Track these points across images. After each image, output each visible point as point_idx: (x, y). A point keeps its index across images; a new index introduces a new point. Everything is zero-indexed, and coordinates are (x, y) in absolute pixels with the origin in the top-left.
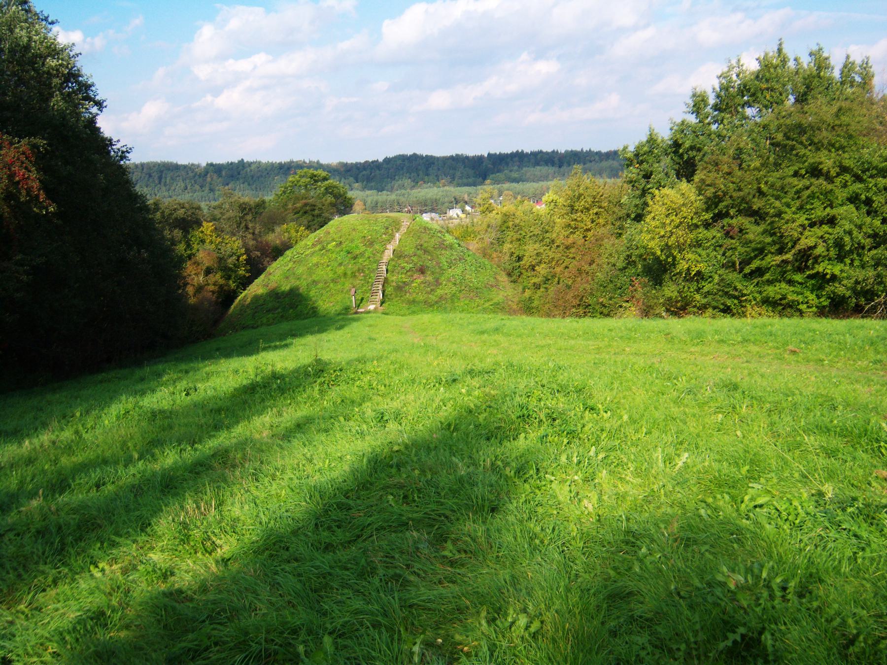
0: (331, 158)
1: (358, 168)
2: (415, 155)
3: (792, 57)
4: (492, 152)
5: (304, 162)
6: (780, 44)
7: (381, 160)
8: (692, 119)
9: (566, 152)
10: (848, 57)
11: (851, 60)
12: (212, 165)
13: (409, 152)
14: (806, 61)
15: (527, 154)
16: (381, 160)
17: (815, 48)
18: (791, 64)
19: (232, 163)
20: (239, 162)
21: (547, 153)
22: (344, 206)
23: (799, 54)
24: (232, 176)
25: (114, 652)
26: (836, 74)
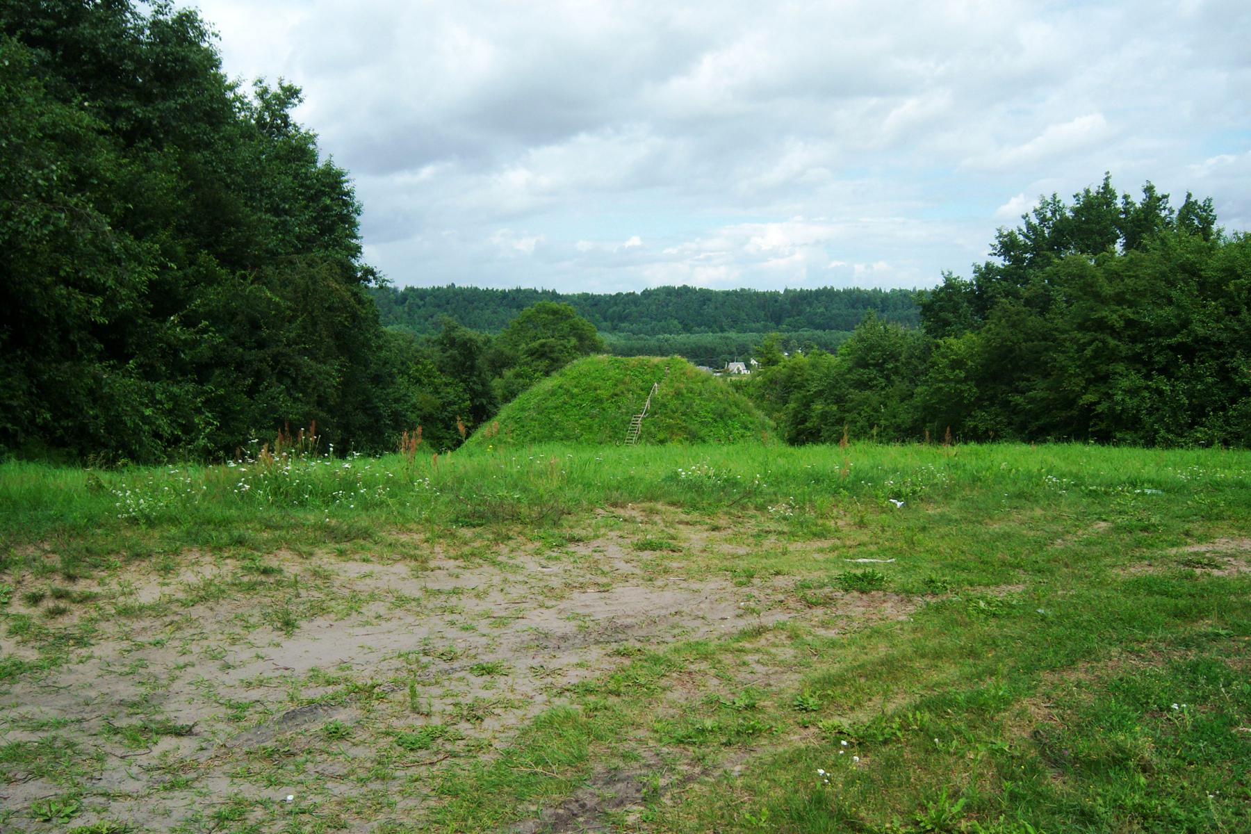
0: (568, 287)
1: (606, 302)
2: (685, 287)
3: (1119, 194)
4: (791, 288)
5: (536, 291)
6: (1107, 179)
7: (639, 292)
8: (999, 262)
9: (893, 291)
10: (1189, 196)
11: (1192, 200)
12: (412, 289)
13: (677, 284)
14: (1138, 199)
15: (838, 291)
16: (639, 292)
17: (1146, 184)
18: (1119, 203)
19: (439, 289)
20: (449, 287)
21: (866, 292)
22: (588, 346)
23: (1129, 192)
24: (439, 306)
25: (508, 753)
26: (257, 104)
